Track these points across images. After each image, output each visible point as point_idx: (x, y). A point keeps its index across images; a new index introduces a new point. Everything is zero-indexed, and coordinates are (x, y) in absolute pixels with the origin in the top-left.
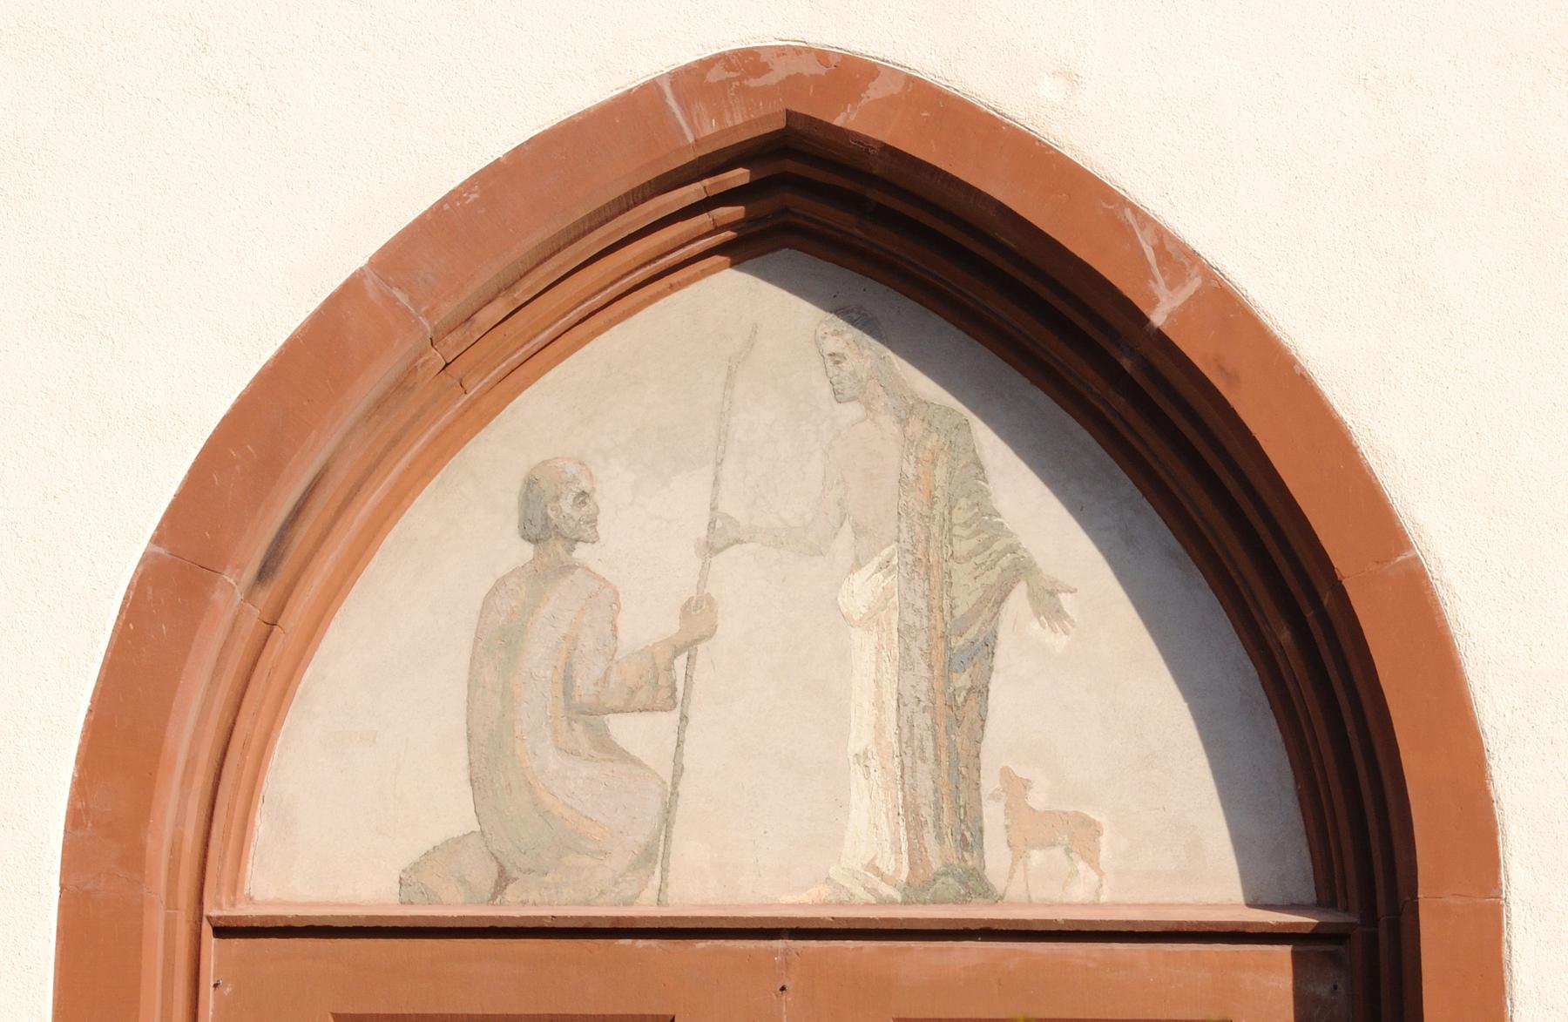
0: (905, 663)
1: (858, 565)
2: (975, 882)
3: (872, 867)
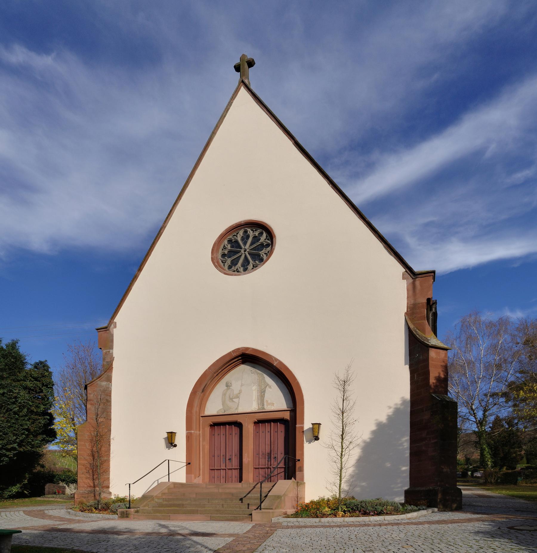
0: (258, 393)
1: (254, 386)
2: (264, 408)
3: (255, 408)
